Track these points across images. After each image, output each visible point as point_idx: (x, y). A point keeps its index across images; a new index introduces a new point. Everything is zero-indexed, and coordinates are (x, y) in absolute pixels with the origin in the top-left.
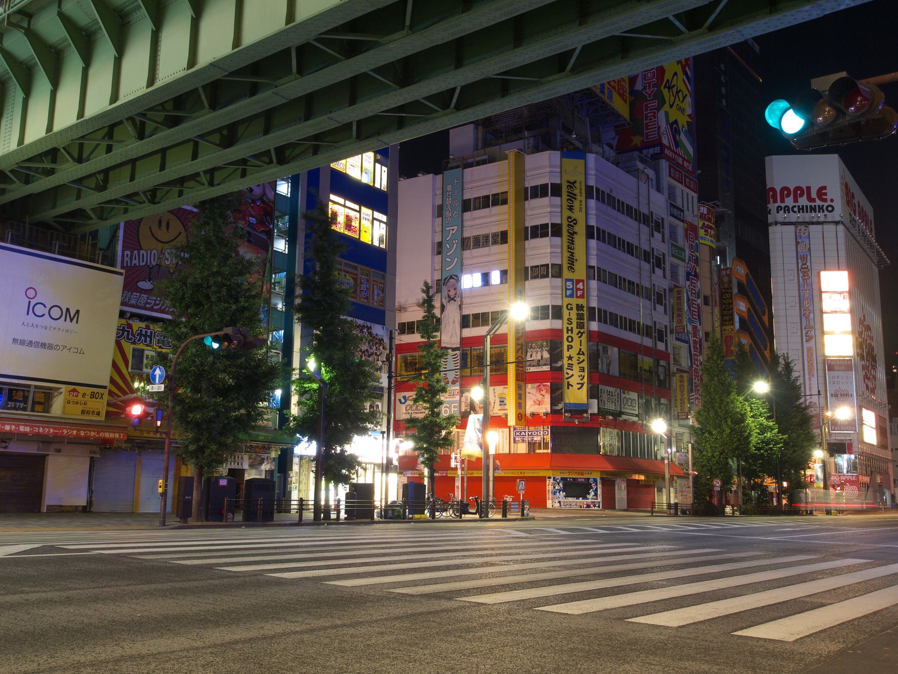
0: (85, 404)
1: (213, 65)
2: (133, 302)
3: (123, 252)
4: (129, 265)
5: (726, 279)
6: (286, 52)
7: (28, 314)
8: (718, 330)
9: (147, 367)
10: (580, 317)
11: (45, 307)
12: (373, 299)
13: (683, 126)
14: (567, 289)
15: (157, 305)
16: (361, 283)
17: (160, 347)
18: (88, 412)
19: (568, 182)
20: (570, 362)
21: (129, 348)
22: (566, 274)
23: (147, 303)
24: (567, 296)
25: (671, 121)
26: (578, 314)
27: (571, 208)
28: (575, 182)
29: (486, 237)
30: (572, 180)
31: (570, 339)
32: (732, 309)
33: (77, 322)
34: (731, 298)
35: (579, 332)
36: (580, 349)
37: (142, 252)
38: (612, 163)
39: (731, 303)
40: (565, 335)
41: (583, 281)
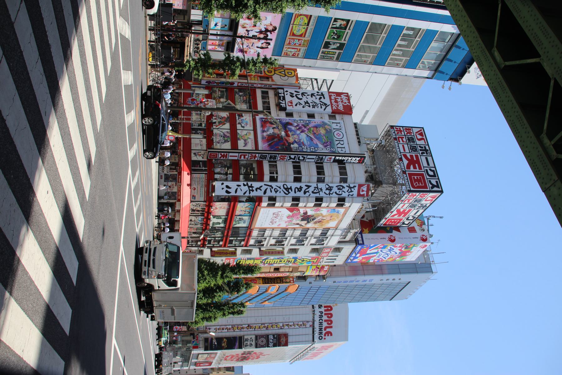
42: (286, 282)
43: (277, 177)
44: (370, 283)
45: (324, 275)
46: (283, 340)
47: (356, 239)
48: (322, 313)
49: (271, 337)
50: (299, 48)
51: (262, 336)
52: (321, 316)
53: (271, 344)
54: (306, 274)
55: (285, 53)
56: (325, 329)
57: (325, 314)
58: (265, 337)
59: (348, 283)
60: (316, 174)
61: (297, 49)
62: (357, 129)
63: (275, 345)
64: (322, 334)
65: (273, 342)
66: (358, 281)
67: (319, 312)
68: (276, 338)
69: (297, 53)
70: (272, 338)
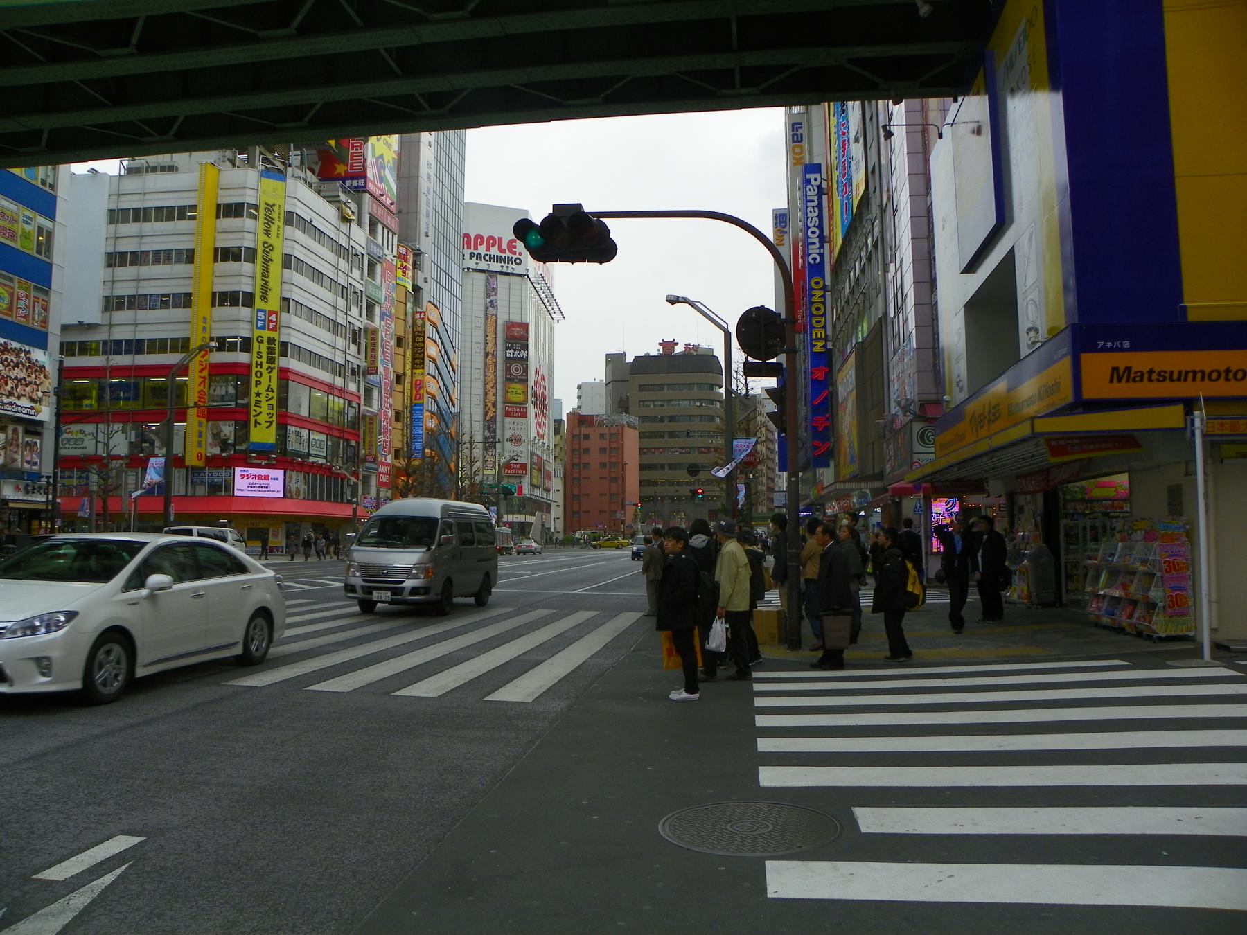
5: (419, 322)
8: (408, 373)
10: (271, 351)
12: (33, 319)
13: (389, 162)
14: (258, 320)
16: (19, 298)
19: (266, 204)
20: (258, 398)
22: (259, 303)
24: (257, 328)
26: (269, 348)
27: (267, 233)
30: (270, 202)
31: (259, 374)
32: (423, 353)
34: (424, 342)
35: (269, 367)
36: (269, 386)
40: (254, 370)
41: (276, 313)
42: (423, 325)
43: (241, 337)
44: (432, 167)
45: (414, 254)
46: (516, 331)
47: (354, 191)
48: (474, 253)
49: (510, 353)
50: (32, 299)
51: (507, 369)
52: (479, 257)
53: (523, 354)
54: (410, 288)
55: (41, 326)
56: (504, 252)
57: (476, 248)
58: (508, 365)
59: (431, 209)
60: (238, 263)
61: (34, 302)
62: (159, 169)
63: (526, 348)
64: (512, 258)
65: (518, 350)
66: (428, 190)
67: (471, 259)
68: (512, 344)
69: (41, 302)
70: (512, 351)
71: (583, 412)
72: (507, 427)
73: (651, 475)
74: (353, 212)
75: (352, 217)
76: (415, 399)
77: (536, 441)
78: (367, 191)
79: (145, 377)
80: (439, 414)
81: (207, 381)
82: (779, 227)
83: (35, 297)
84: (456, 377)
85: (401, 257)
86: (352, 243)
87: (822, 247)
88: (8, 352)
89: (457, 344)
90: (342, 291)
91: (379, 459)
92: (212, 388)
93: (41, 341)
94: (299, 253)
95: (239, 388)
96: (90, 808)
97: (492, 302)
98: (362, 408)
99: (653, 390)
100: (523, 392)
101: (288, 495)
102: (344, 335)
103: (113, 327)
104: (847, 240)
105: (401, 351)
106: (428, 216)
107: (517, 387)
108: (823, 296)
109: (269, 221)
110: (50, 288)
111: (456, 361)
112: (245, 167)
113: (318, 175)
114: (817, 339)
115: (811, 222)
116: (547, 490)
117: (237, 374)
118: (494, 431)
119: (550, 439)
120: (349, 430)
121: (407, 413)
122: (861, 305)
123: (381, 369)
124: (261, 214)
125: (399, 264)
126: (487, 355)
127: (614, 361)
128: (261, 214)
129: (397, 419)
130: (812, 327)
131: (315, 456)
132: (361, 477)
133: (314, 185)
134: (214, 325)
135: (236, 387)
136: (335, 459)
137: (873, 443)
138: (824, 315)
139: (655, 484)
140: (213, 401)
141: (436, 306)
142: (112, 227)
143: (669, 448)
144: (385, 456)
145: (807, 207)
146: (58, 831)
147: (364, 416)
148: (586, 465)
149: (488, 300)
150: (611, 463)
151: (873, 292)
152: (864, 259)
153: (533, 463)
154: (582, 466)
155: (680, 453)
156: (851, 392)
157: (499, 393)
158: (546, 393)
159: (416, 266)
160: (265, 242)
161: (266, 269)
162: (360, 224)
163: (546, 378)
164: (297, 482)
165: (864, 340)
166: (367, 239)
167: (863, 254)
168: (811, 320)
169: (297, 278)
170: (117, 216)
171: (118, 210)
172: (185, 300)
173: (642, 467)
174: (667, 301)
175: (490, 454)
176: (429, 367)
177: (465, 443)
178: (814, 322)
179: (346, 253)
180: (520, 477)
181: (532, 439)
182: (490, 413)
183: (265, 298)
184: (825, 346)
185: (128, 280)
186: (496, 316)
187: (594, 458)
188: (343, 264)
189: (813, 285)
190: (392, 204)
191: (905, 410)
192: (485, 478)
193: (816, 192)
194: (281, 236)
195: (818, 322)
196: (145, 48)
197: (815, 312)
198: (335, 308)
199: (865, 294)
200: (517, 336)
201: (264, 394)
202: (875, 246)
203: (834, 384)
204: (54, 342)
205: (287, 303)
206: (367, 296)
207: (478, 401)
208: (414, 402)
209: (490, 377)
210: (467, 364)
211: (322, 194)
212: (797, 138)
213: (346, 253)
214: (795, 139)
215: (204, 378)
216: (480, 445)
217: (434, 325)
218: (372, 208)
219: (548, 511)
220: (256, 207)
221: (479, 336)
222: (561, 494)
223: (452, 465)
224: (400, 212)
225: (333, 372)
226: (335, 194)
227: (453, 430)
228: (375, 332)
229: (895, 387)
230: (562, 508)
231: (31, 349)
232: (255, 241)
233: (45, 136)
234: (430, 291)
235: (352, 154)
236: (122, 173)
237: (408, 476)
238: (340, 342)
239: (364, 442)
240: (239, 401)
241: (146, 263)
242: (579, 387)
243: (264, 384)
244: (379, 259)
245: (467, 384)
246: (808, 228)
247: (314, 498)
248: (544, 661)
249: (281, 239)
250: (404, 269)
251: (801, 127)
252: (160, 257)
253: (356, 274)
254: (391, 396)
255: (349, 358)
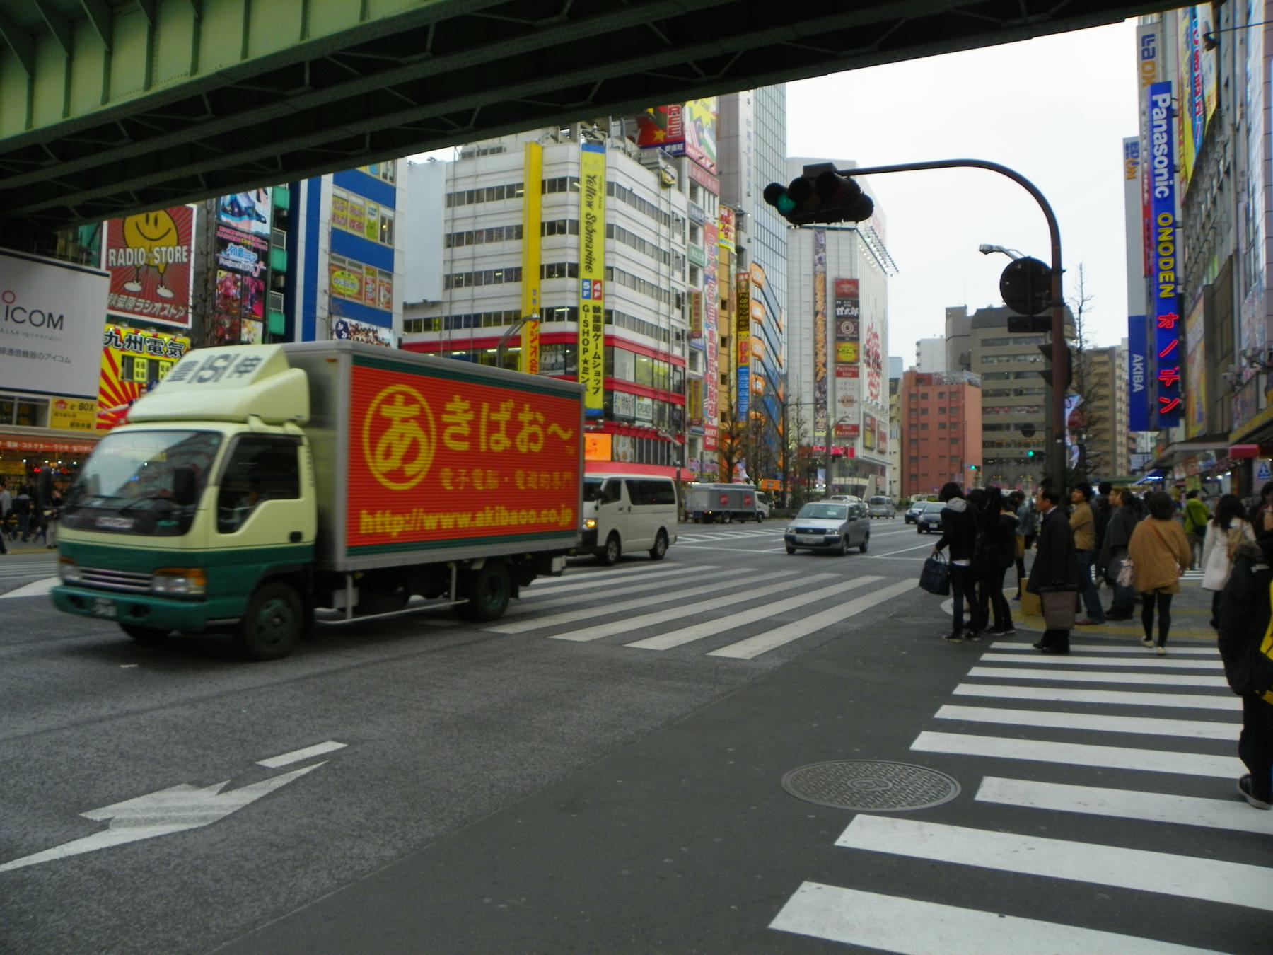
0: (74, 416)
1: (220, 74)
2: (120, 305)
3: (108, 251)
4: (114, 264)
5: (743, 284)
6: (300, 66)
7: (6, 319)
8: (734, 335)
9: (138, 376)
10: (597, 319)
11: (25, 311)
12: (379, 301)
13: (707, 124)
14: (584, 290)
15: (147, 308)
16: (366, 283)
17: (152, 354)
18: (78, 425)
19: (588, 176)
20: (585, 365)
21: (117, 355)
22: (583, 273)
23: (136, 306)
24: (583, 297)
25: (695, 117)
26: (595, 317)
27: (590, 205)
28: (594, 177)
29: (500, 230)
30: (592, 174)
31: (586, 342)
32: (748, 314)
33: (61, 328)
34: (748, 303)
35: (596, 335)
36: (596, 353)
37: (129, 250)
38: (634, 159)
39: (748, 309)
40: (581, 338)
41: (600, 282)
44: (752, 124)
46: (846, 288)
49: (840, 311)
51: (838, 328)
53: (854, 312)
54: (733, 250)
59: (752, 169)
60: (563, 236)
61: (380, 286)
63: (856, 304)
71: (923, 370)
72: (839, 387)
73: (994, 436)
74: (673, 178)
75: (673, 182)
76: (741, 361)
77: (869, 402)
78: (685, 155)
79: (482, 349)
80: (768, 378)
81: (538, 351)
82: (1130, 159)
83: (380, 281)
84: (783, 338)
85: (724, 219)
86: (673, 209)
87: (1171, 177)
88: (359, 332)
89: (783, 303)
90: (665, 257)
91: (706, 422)
92: (543, 358)
93: (385, 319)
94: (620, 222)
95: (568, 357)
96: (320, 721)
97: (820, 259)
98: (688, 372)
99: (998, 345)
100: (855, 351)
101: (616, 458)
102: (667, 299)
103: (575, 290)
104: (1198, 168)
105: (725, 313)
106: (749, 175)
107: (848, 346)
108: (1173, 234)
109: (591, 192)
110: (392, 271)
111: (783, 322)
112: (567, 141)
113: (639, 143)
114: (1165, 283)
115: (1158, 150)
116: (882, 452)
117: (566, 343)
118: (825, 392)
119: (884, 399)
120: (674, 394)
121: (733, 376)
122: (1212, 242)
123: (705, 332)
124: (583, 186)
125: (721, 226)
126: (816, 313)
127: (955, 315)
128: (583, 186)
129: (723, 382)
130: (1160, 270)
131: (641, 420)
132: (687, 441)
133: (633, 154)
134: (543, 297)
135: (565, 355)
136: (661, 423)
137: (1222, 399)
138: (1174, 255)
139: (1000, 445)
140: (544, 369)
141: (760, 267)
142: (450, 210)
143: (1014, 407)
144: (711, 420)
145: (1153, 134)
146: (288, 734)
147: (689, 381)
148: (925, 426)
149: (817, 257)
150: (951, 424)
151: (1225, 227)
152: (1215, 190)
153: (865, 424)
154: (920, 427)
155: (1028, 412)
156: (1199, 341)
157: (830, 352)
158: (880, 351)
159: (738, 227)
160: (588, 214)
161: (590, 240)
162: (680, 189)
163: (879, 336)
164: (624, 445)
165: (1215, 281)
166: (688, 203)
167: (1215, 182)
168: (1157, 264)
169: (619, 246)
170: (454, 199)
171: (455, 194)
172: (514, 275)
173: (986, 428)
174: (980, 251)
175: (822, 415)
176: (755, 328)
177: (791, 405)
178: (1161, 263)
179: (667, 219)
180: (852, 438)
181: (865, 399)
182: (821, 374)
183: (590, 268)
184: (1174, 290)
185: (467, 259)
186: (825, 273)
187: (933, 418)
188: (664, 230)
189: (1160, 222)
190: (712, 166)
191: (1251, 361)
192: (816, 440)
193: (1165, 115)
194: (602, 206)
195: (1166, 264)
196: (438, 52)
197: (1161, 252)
198: (658, 274)
199: (1215, 229)
200: (847, 293)
201: (591, 361)
202: (1227, 172)
203: (1184, 334)
204: (398, 321)
205: (610, 271)
206: (690, 260)
207: (808, 361)
208: (740, 364)
209: (820, 336)
210: (797, 324)
211: (642, 162)
212: (1149, 53)
213: (667, 219)
214: (1146, 55)
215: (535, 348)
216: (811, 407)
217: (759, 286)
218: (692, 171)
219: (883, 474)
220: (578, 180)
221: (808, 295)
222: (898, 457)
223: (780, 428)
224: (720, 173)
225: (657, 337)
226: (654, 160)
227: (781, 392)
228: (698, 296)
229: (1245, 334)
230: (898, 472)
231: (378, 328)
232: (579, 213)
233: (368, 138)
234: (754, 252)
235: (670, 119)
236: (457, 159)
237: (733, 438)
238: (664, 307)
239: (690, 406)
240: (568, 369)
241: (480, 241)
242: (918, 344)
243: (592, 349)
244: (701, 223)
245: (797, 344)
246: (1155, 157)
247: (641, 461)
248: (790, 622)
249: (603, 209)
250: (726, 231)
251: (1153, 41)
252: (493, 235)
253: (678, 238)
254: (716, 359)
255: (673, 323)
